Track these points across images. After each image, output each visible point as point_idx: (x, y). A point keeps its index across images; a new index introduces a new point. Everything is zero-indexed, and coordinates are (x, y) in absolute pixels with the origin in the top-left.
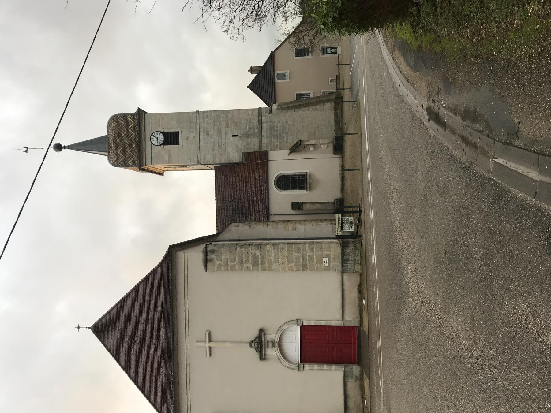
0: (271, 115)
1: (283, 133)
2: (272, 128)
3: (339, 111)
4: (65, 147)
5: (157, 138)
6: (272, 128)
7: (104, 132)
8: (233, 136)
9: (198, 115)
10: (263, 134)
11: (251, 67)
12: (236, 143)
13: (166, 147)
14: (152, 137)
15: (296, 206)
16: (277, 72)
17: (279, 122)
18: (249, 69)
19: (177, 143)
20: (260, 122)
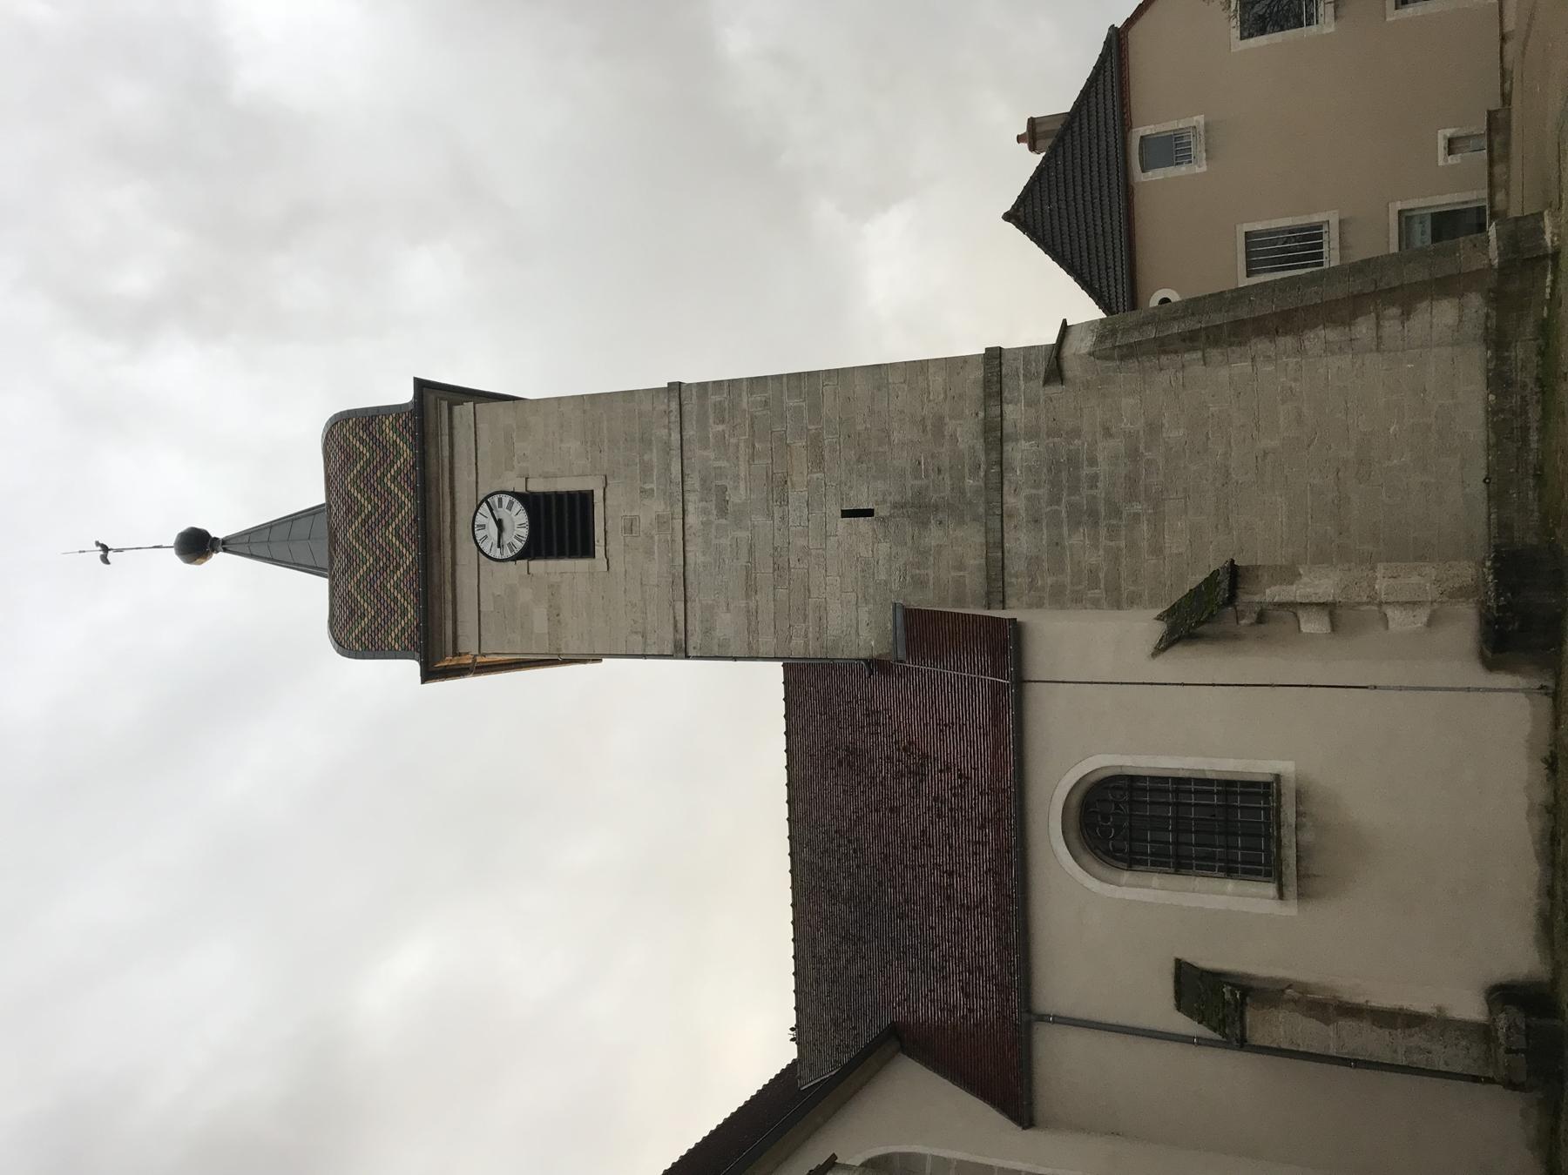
0: (1054, 390)
1: (1132, 497)
2: (1063, 471)
3: (1521, 352)
4: (226, 545)
5: (499, 523)
6: (1063, 471)
7: (313, 493)
8: (846, 514)
9: (674, 406)
10: (1010, 500)
11: (1032, 121)
12: (865, 553)
13: (538, 565)
14: (484, 508)
15: (1216, 1002)
16: (1140, 131)
17: (1108, 433)
18: (1023, 129)
19: (587, 551)
20: (995, 435)
